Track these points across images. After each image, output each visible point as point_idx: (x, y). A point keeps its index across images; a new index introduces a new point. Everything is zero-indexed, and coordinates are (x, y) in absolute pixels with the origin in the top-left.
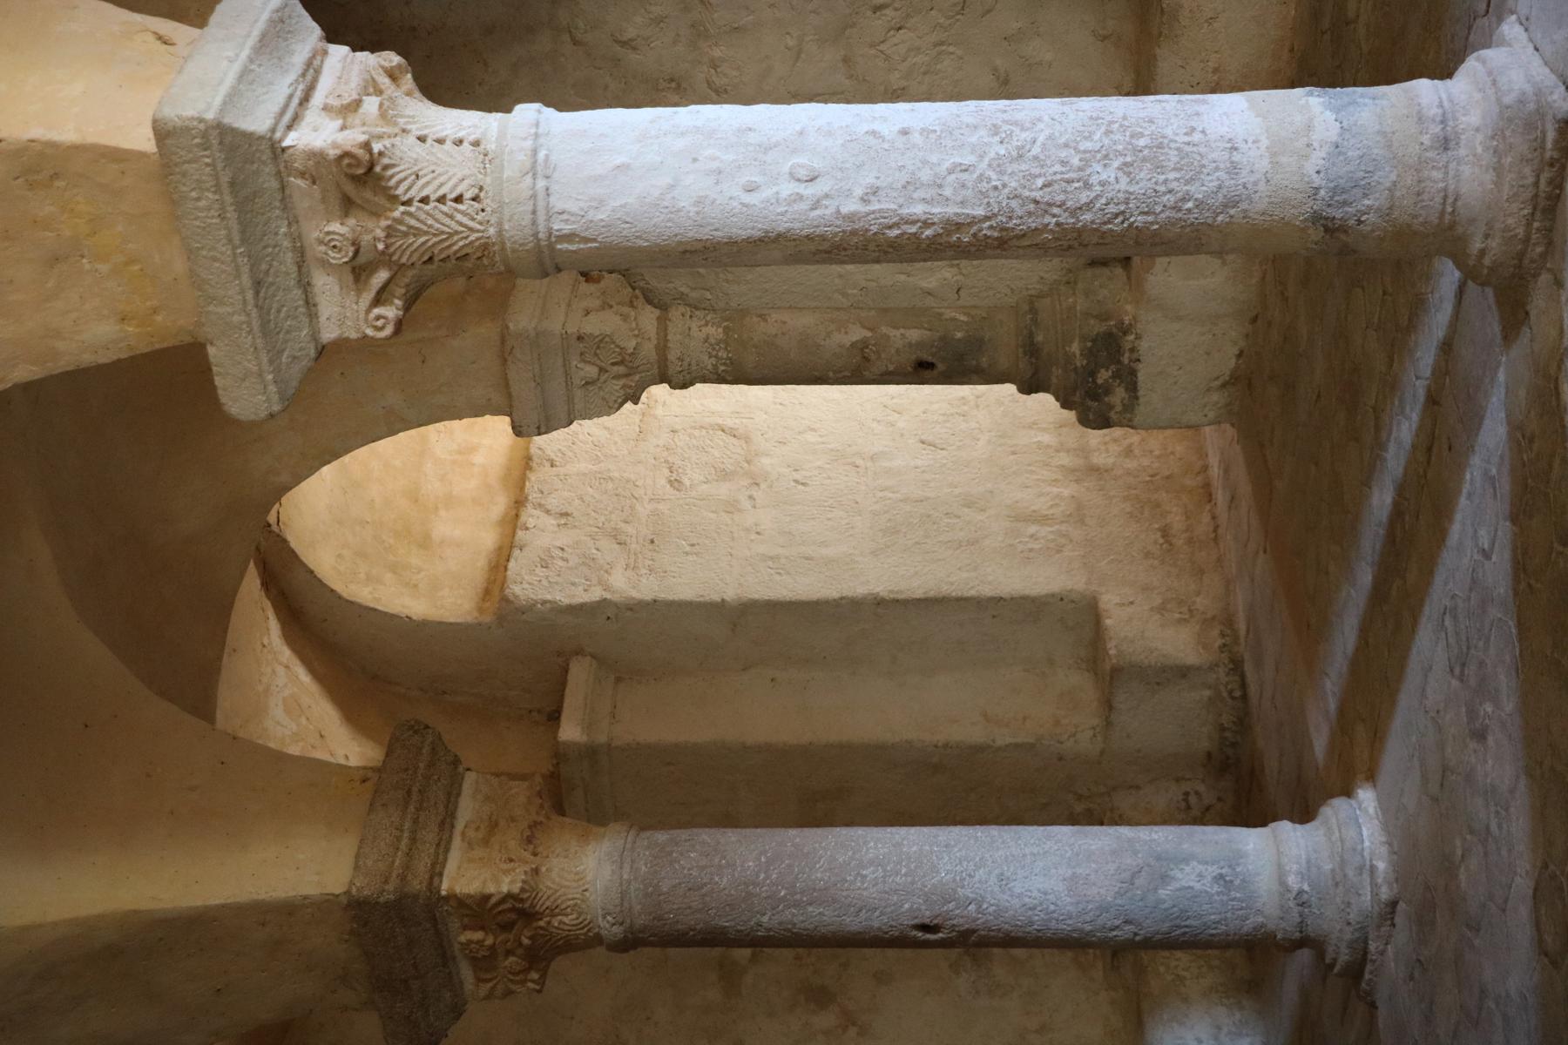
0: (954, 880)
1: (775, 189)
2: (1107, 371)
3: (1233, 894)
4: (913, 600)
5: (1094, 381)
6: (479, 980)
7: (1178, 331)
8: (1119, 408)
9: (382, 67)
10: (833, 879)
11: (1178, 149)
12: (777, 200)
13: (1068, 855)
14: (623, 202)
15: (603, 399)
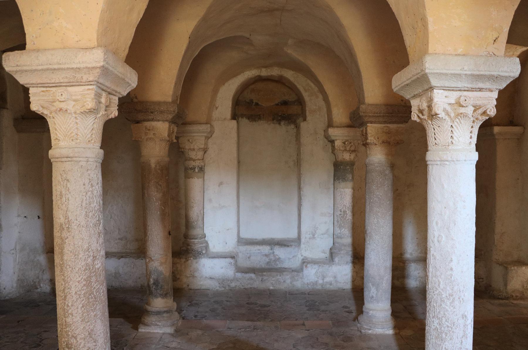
0: (373, 239)
1: (436, 230)
3: (370, 299)
9: (487, 110)
10: (374, 212)
11: (441, 345)
12: (434, 231)
13: (379, 265)
14: (434, 186)
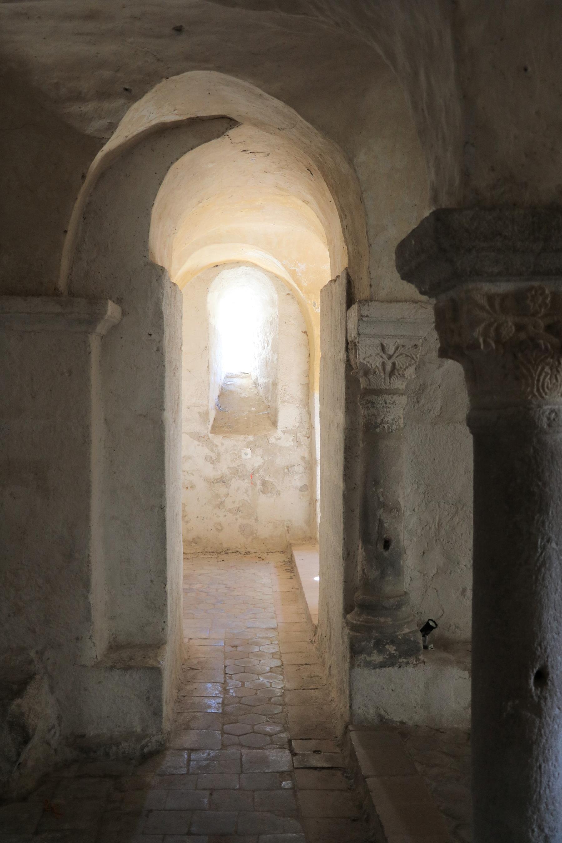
2: (395, 650)
4: (165, 530)
5: (387, 643)
6: (491, 298)
7: (418, 687)
8: (368, 659)
15: (371, 355)
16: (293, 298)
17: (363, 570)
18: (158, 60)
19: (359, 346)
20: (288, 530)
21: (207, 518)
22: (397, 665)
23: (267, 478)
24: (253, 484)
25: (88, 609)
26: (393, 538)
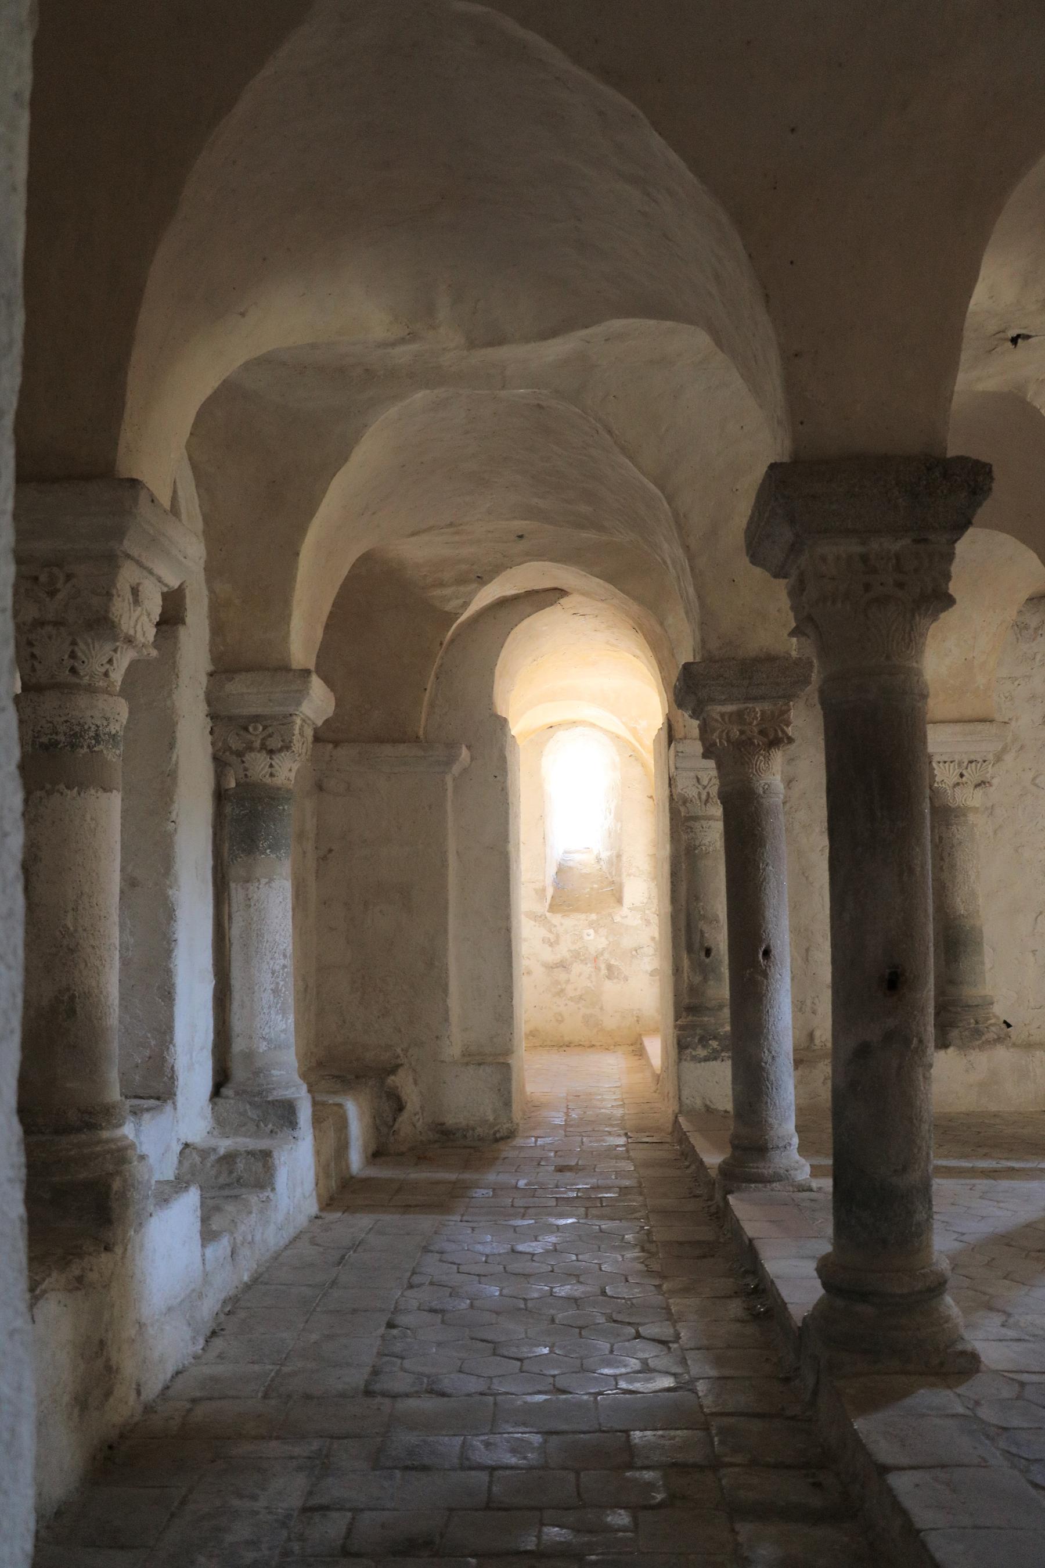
5: (710, 1039)
6: (722, 715)
8: (694, 1053)
16: (637, 760)
17: (689, 977)
18: (504, 556)
19: (678, 779)
20: (638, 1021)
21: (545, 1008)
22: (720, 1059)
23: (613, 962)
24: (598, 969)
25: (447, 1010)
26: (713, 947)
